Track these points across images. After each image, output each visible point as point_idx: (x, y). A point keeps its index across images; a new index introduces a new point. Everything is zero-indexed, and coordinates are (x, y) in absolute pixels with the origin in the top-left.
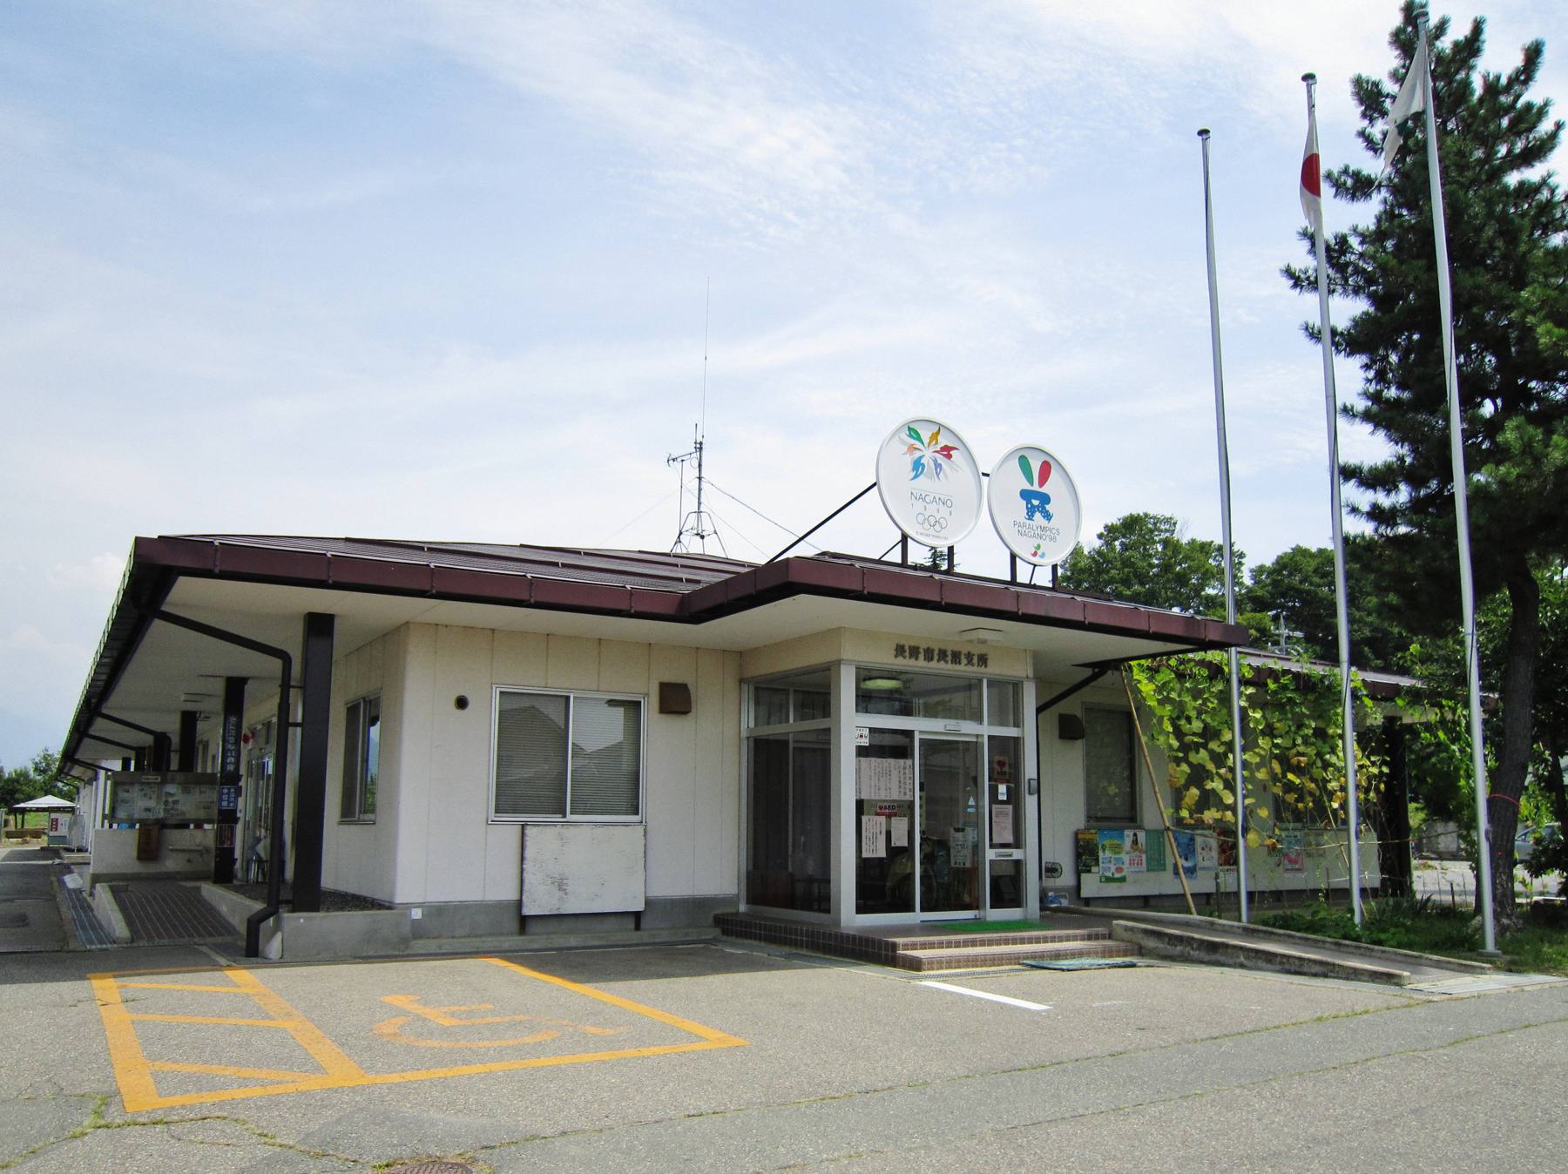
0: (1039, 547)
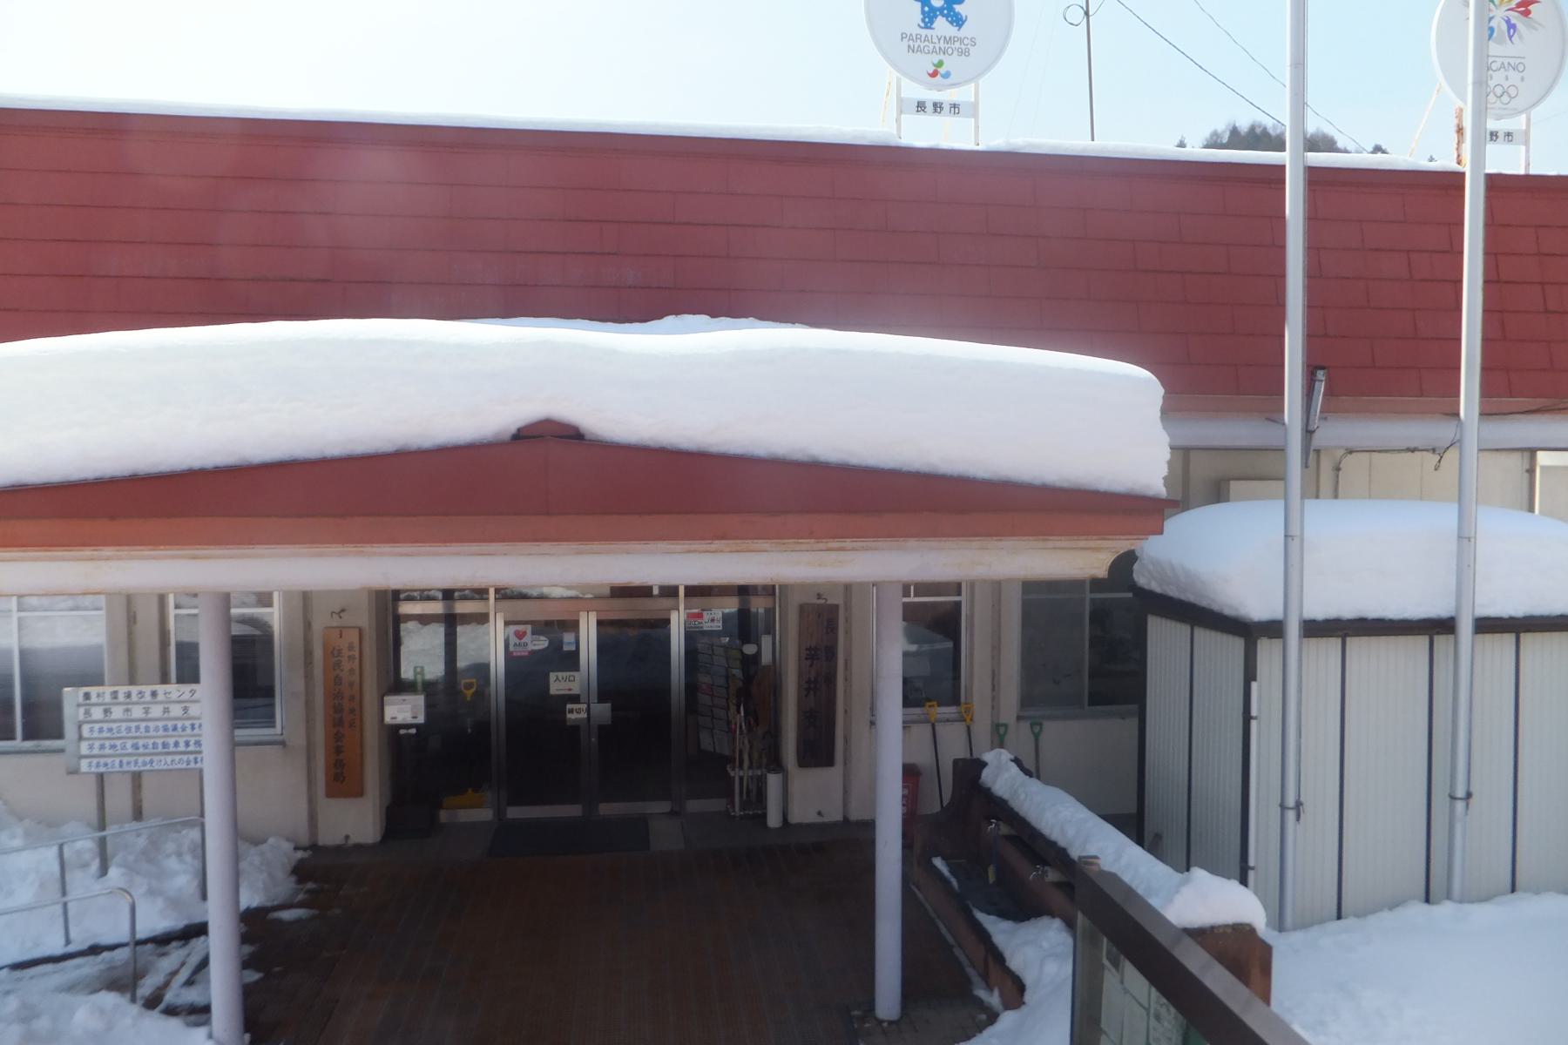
0: (940, 64)
